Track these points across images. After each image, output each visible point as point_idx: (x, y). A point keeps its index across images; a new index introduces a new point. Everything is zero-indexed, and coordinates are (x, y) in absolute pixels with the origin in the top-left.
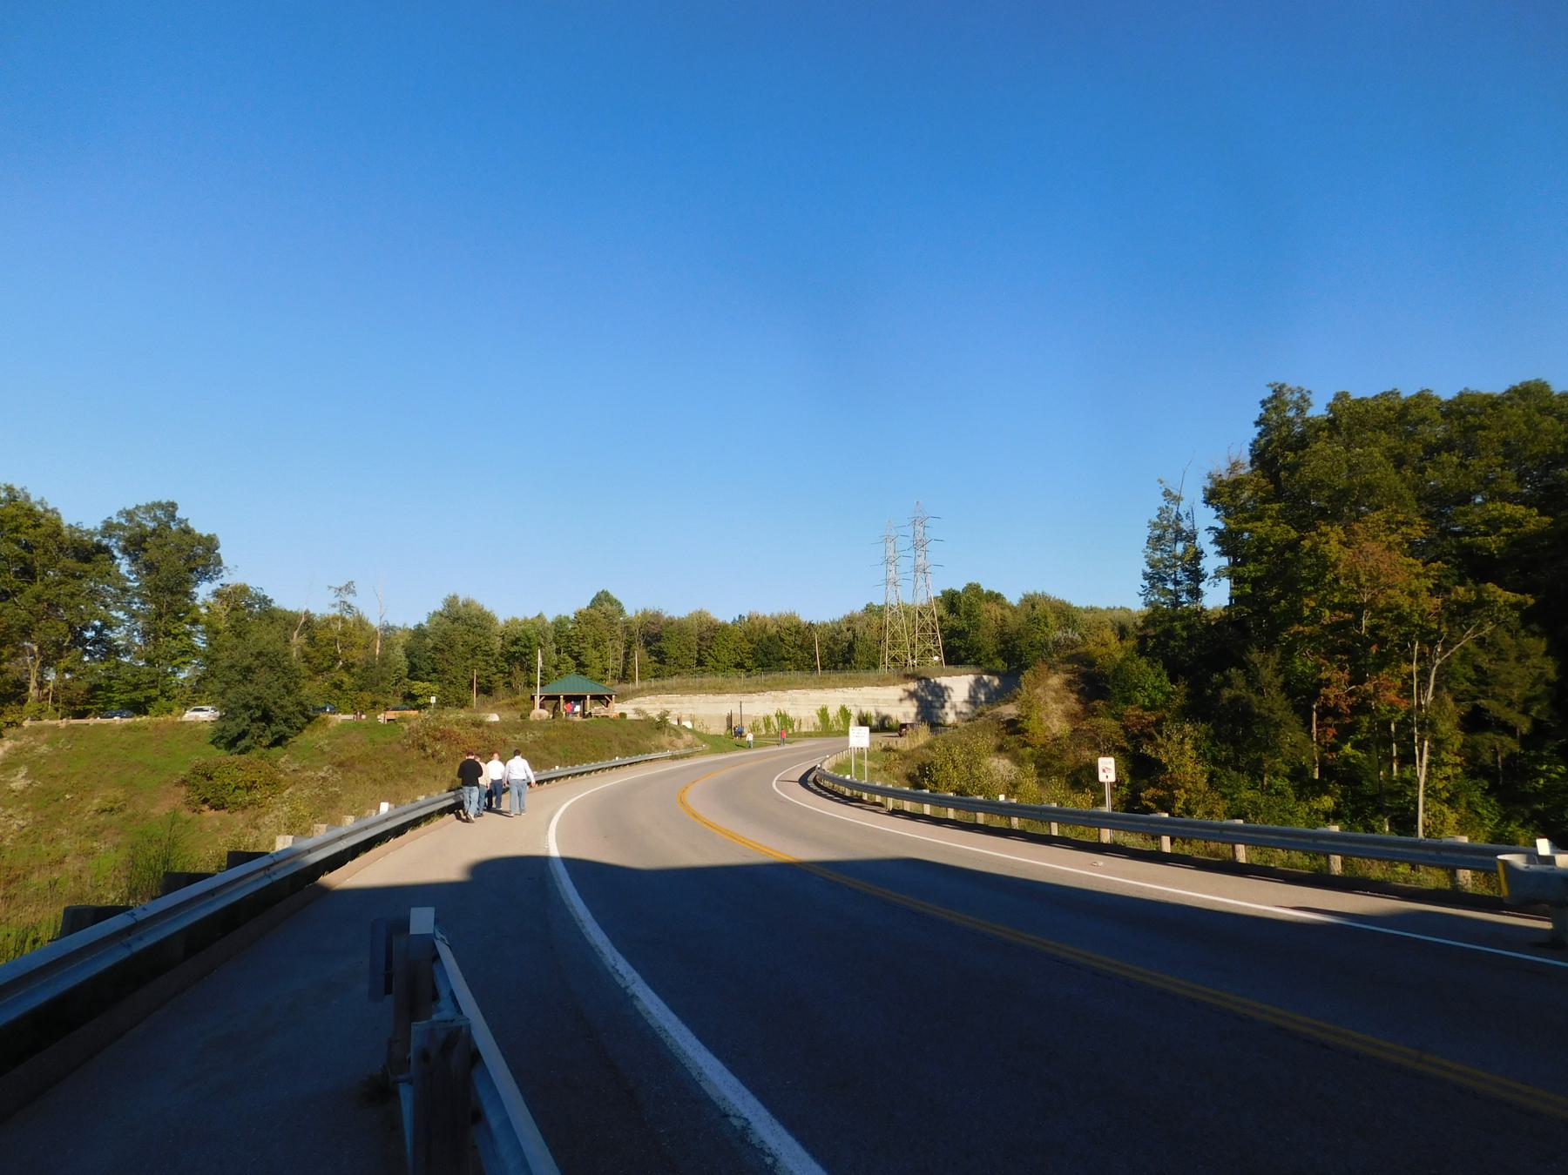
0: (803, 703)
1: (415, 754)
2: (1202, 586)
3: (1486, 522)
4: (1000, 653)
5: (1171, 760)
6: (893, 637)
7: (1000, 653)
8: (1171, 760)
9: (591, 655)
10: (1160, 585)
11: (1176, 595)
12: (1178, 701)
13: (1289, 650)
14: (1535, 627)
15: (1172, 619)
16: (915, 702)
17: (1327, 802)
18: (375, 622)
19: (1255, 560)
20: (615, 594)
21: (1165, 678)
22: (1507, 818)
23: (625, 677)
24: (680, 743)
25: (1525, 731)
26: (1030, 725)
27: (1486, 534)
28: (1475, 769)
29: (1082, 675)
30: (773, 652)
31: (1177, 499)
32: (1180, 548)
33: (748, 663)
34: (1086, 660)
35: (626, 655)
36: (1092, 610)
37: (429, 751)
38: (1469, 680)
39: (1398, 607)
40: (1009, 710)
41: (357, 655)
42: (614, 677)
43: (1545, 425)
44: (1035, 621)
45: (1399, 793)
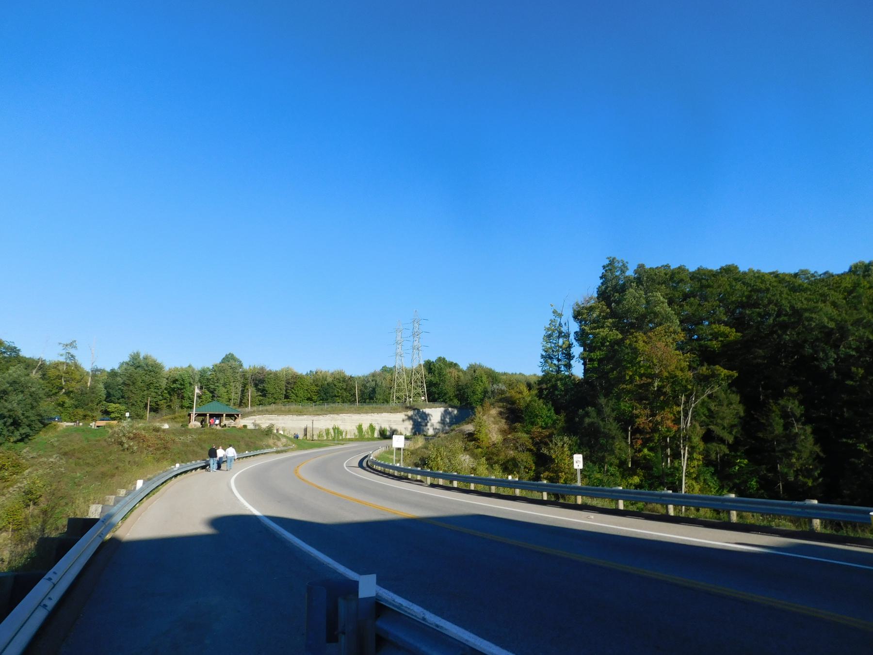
0: (349, 421)
1: (116, 448)
2: (572, 362)
3: (711, 334)
4: (456, 396)
5: (557, 456)
6: (398, 386)
7: (456, 396)
8: (557, 456)
9: (222, 390)
10: (549, 361)
11: (558, 366)
12: (561, 424)
13: (618, 398)
14: (734, 389)
15: (557, 380)
16: (411, 422)
17: (636, 480)
18: (87, 367)
19: (600, 349)
20: (237, 355)
21: (553, 411)
22: (722, 488)
23: (242, 403)
24: (279, 444)
25: (730, 442)
26: (481, 436)
27: (711, 340)
28: (708, 462)
29: (508, 409)
30: (330, 392)
31: (560, 316)
32: (561, 341)
33: (315, 398)
34: (510, 401)
35: (243, 391)
36: (505, 374)
37: (126, 446)
38: (705, 415)
39: (676, 376)
40: (469, 428)
41: (75, 386)
42: (234, 404)
43: (738, 287)
44: (476, 379)
45: (672, 475)
